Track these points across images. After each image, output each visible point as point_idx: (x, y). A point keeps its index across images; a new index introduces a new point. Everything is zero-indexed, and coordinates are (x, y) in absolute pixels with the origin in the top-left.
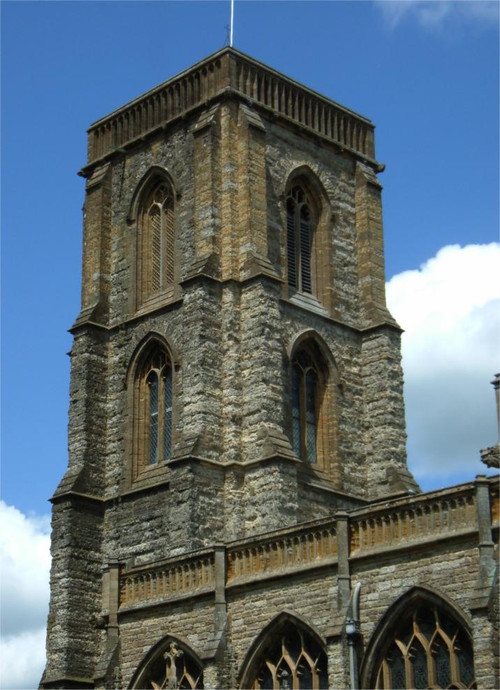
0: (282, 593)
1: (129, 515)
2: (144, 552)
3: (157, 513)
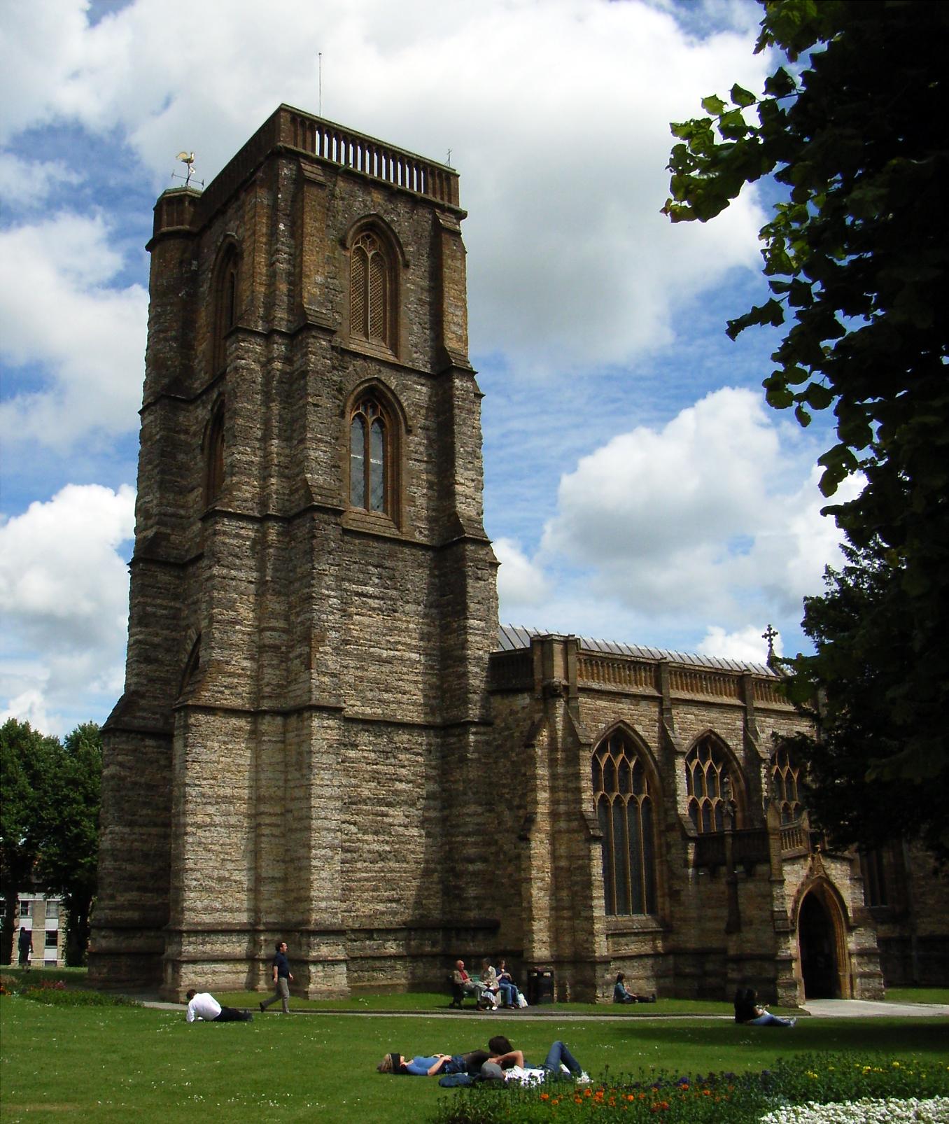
0: (714, 714)
1: (352, 552)
2: (370, 597)
3: (387, 563)
